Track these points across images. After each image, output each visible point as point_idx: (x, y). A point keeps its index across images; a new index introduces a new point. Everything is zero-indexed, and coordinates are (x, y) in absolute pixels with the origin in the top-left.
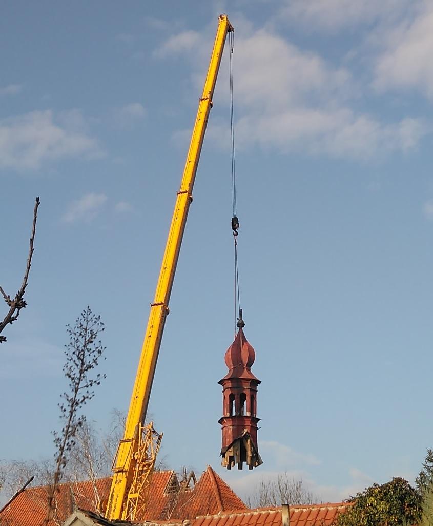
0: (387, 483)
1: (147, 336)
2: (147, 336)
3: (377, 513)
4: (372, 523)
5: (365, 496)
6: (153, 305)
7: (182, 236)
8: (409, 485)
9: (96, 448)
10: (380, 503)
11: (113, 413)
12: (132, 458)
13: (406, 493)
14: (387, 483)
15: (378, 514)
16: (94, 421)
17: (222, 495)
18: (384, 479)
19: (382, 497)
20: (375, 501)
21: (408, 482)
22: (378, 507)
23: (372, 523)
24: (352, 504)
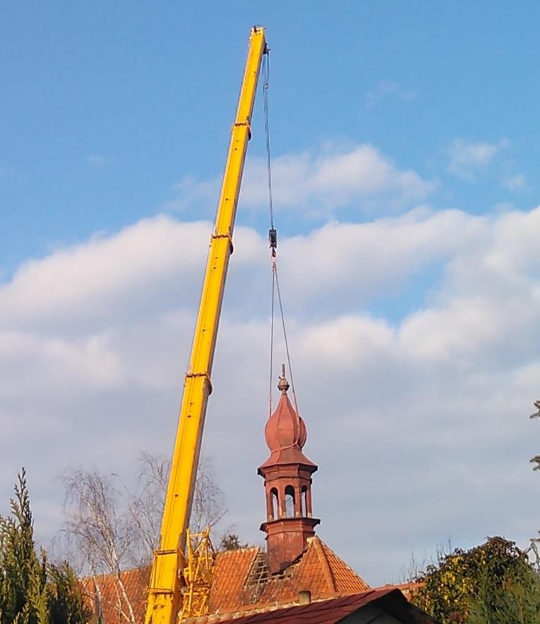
0: (476, 547)
1: (183, 415)
2: (183, 415)
3: (456, 598)
4: (442, 614)
5: (440, 571)
6: (191, 377)
7: (205, 412)
8: (516, 548)
9: (116, 518)
10: (461, 580)
11: (142, 460)
12: (179, 576)
13: (508, 562)
14: (476, 547)
15: (458, 598)
16: (113, 474)
17: (337, 577)
18: (472, 542)
19: (465, 571)
20: (454, 578)
21: (514, 543)
22: (457, 587)
23: (442, 614)
24: (423, 584)
